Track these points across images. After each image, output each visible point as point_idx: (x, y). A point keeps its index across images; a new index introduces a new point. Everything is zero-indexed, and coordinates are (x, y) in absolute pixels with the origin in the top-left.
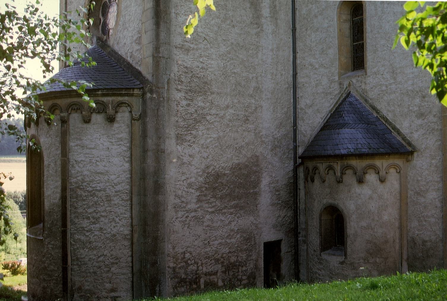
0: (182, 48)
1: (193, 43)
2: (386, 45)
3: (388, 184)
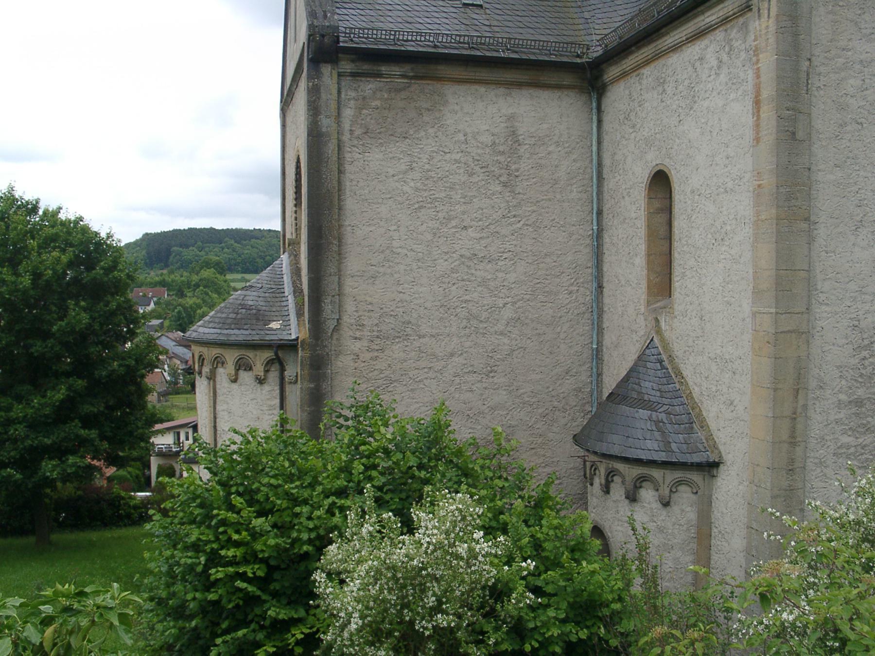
0: (363, 276)
1: (383, 266)
2: (695, 269)
3: (675, 509)
